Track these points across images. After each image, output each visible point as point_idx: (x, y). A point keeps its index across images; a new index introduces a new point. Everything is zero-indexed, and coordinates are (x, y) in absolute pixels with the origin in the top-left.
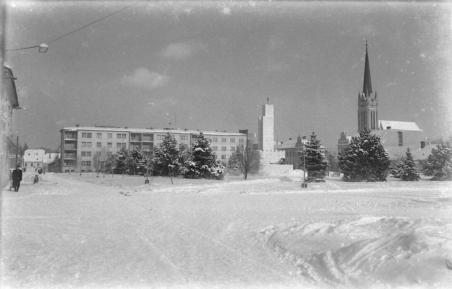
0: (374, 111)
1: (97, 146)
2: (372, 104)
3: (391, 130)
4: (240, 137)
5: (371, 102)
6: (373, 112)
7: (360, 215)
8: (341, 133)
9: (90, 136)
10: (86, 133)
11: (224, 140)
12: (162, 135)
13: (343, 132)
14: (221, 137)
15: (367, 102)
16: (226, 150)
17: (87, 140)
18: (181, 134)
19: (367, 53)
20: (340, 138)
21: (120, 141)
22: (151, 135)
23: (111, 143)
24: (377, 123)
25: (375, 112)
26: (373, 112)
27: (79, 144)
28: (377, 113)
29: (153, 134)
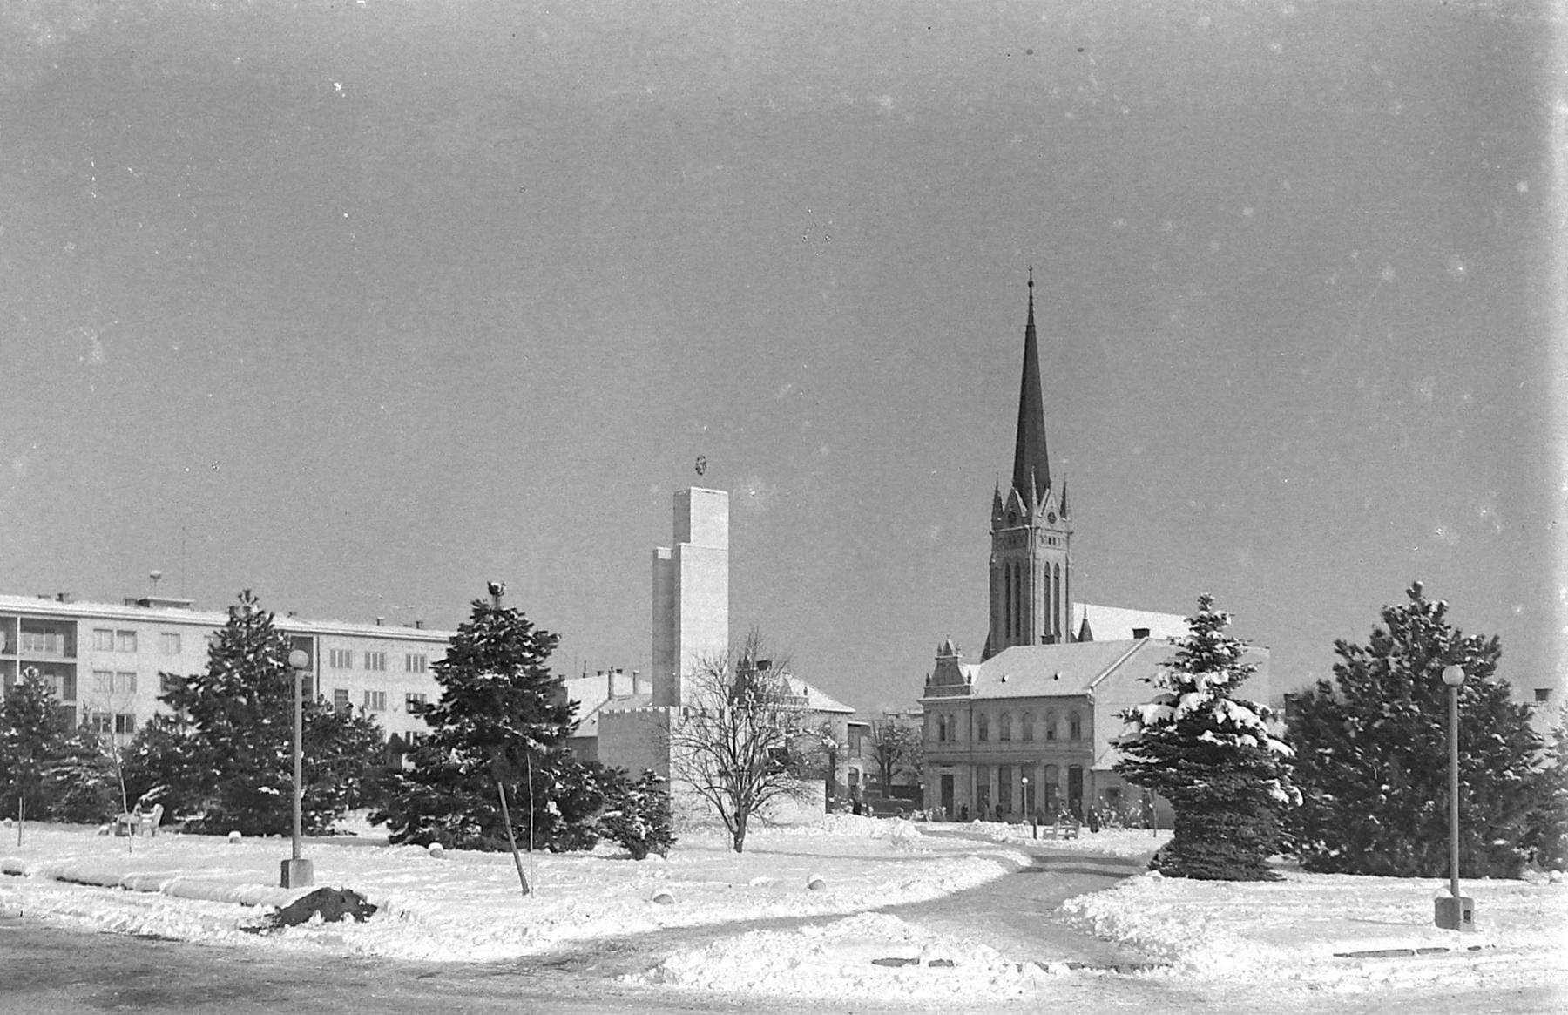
0: (1057, 565)
2: (1049, 534)
3: (1153, 643)
5: (1045, 524)
6: (1052, 568)
8: (939, 650)
12: (119, 632)
13: (947, 644)
15: (1030, 524)
19: (1031, 318)
20: (931, 668)
22: (66, 627)
24: (1067, 613)
25: (1062, 566)
26: (1052, 568)
28: (1070, 572)
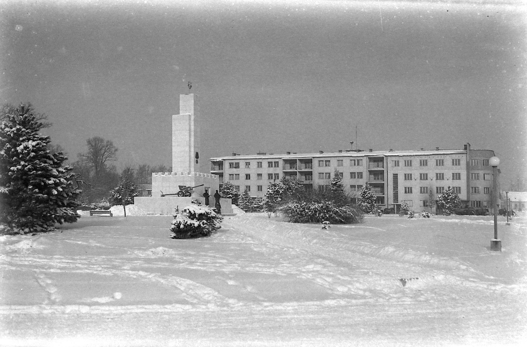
1: (351, 177)
4: (454, 157)
7: (190, 322)
9: (237, 166)
10: (323, 161)
11: (260, 165)
14: (418, 159)
16: (427, 179)
17: (234, 171)
18: (351, 156)
21: (272, 170)
23: (261, 174)
27: (315, 176)
29: (312, 159)
